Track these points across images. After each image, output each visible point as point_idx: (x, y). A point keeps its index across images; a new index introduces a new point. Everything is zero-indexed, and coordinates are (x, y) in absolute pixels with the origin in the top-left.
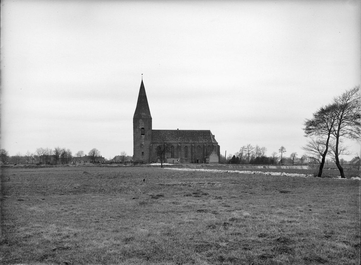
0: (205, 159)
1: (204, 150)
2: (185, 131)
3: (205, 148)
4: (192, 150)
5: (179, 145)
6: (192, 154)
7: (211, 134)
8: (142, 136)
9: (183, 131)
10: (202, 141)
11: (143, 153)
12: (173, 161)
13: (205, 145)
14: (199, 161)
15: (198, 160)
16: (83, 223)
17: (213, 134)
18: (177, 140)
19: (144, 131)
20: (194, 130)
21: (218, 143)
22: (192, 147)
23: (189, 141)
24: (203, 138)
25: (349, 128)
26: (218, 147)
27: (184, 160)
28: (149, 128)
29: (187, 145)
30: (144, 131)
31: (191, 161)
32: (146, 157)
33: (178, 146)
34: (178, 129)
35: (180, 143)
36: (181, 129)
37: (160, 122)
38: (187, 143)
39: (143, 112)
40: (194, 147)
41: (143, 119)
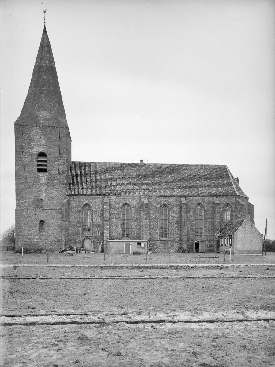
0: (218, 241)
1: (214, 215)
2: (161, 165)
3: (217, 211)
4: (180, 217)
5: (145, 201)
6: (180, 227)
7: (230, 173)
8: (41, 174)
9: (155, 165)
10: (205, 190)
11: (42, 222)
12: (128, 246)
13: (217, 202)
14: (201, 247)
15: (197, 244)
16: (164, 350)
17: (235, 177)
18: (140, 187)
19: (45, 161)
20: (183, 165)
21: (248, 198)
22: (181, 208)
23: (173, 191)
24: (210, 183)
25: (135, 280)
26: (249, 210)
27: (159, 244)
28: (60, 154)
29: (165, 201)
30: (45, 161)
31: (178, 246)
32: (52, 234)
33: (142, 205)
34: (142, 161)
35: (146, 196)
36: (148, 160)
37: (99, 136)
38: (167, 196)
39: (44, 110)
40: (187, 208)
41: (42, 128)
